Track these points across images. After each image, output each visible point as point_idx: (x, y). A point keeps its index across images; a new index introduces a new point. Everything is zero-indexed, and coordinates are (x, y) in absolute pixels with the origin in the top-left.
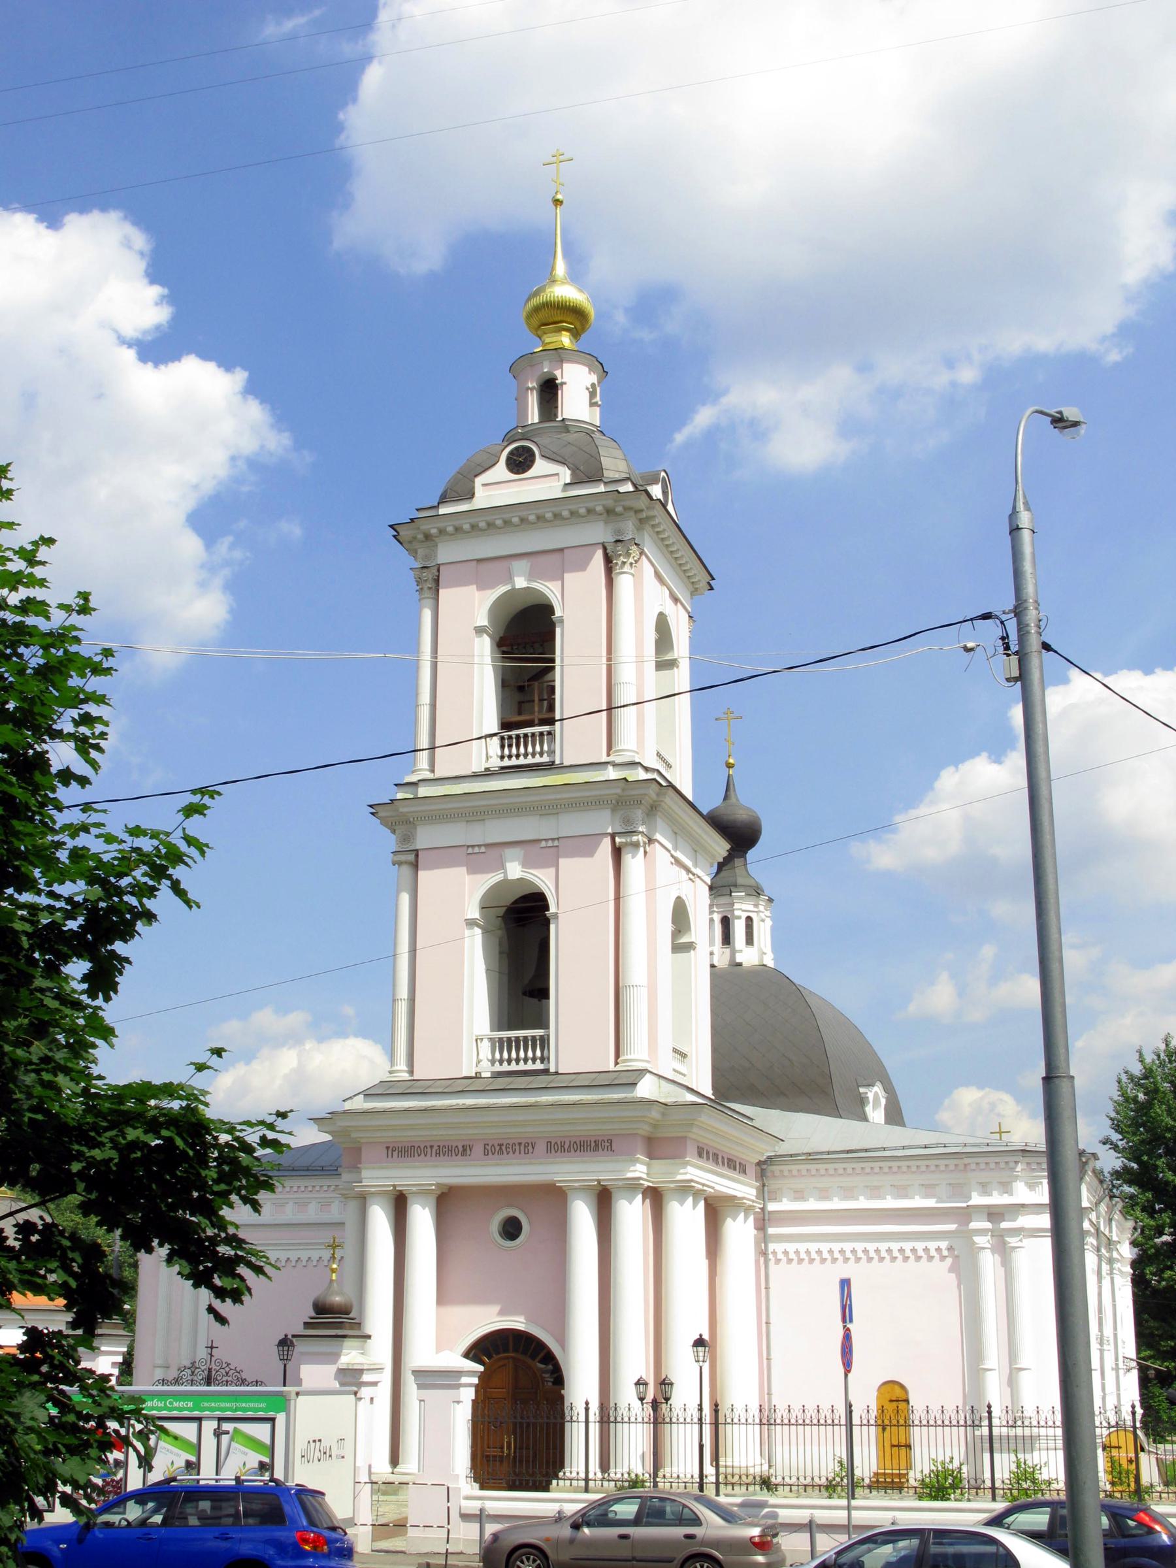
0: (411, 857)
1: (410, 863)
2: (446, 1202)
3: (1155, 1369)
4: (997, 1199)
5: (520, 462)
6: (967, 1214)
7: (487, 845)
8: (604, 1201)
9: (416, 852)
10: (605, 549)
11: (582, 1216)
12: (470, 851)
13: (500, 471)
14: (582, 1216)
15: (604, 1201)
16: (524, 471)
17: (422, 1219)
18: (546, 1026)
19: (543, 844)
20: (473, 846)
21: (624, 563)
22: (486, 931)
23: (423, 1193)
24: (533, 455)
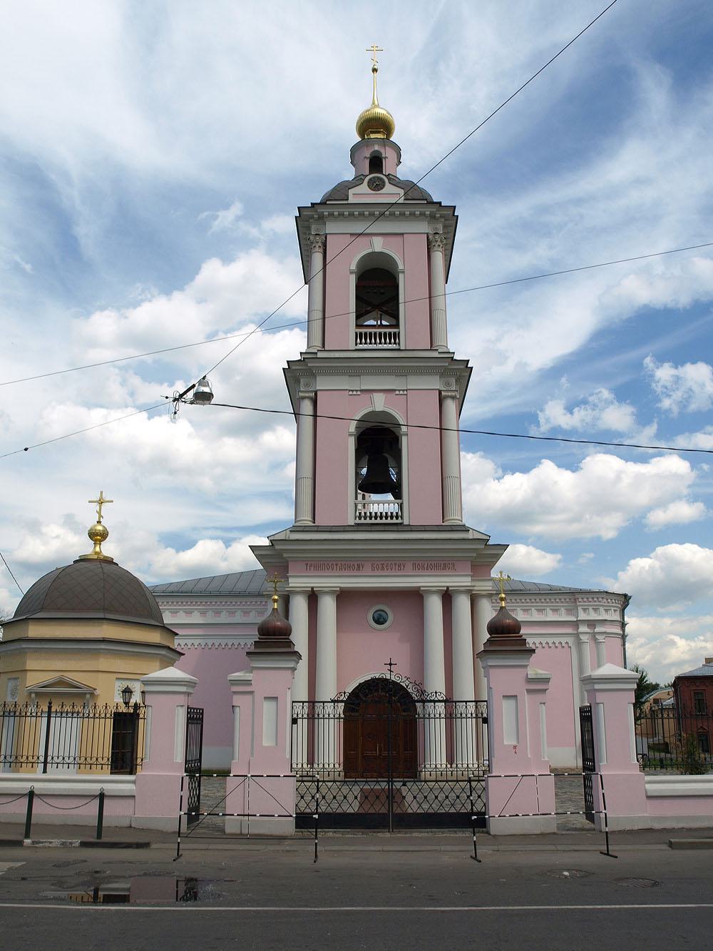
2: (344, 597)
4: (593, 616)
6: (576, 624)
7: (361, 391)
8: (447, 597)
11: (434, 606)
12: (351, 393)
14: (434, 606)
15: (447, 597)
17: (328, 606)
19: (397, 392)
20: (353, 391)
21: (439, 245)
23: (331, 592)
24: (384, 182)
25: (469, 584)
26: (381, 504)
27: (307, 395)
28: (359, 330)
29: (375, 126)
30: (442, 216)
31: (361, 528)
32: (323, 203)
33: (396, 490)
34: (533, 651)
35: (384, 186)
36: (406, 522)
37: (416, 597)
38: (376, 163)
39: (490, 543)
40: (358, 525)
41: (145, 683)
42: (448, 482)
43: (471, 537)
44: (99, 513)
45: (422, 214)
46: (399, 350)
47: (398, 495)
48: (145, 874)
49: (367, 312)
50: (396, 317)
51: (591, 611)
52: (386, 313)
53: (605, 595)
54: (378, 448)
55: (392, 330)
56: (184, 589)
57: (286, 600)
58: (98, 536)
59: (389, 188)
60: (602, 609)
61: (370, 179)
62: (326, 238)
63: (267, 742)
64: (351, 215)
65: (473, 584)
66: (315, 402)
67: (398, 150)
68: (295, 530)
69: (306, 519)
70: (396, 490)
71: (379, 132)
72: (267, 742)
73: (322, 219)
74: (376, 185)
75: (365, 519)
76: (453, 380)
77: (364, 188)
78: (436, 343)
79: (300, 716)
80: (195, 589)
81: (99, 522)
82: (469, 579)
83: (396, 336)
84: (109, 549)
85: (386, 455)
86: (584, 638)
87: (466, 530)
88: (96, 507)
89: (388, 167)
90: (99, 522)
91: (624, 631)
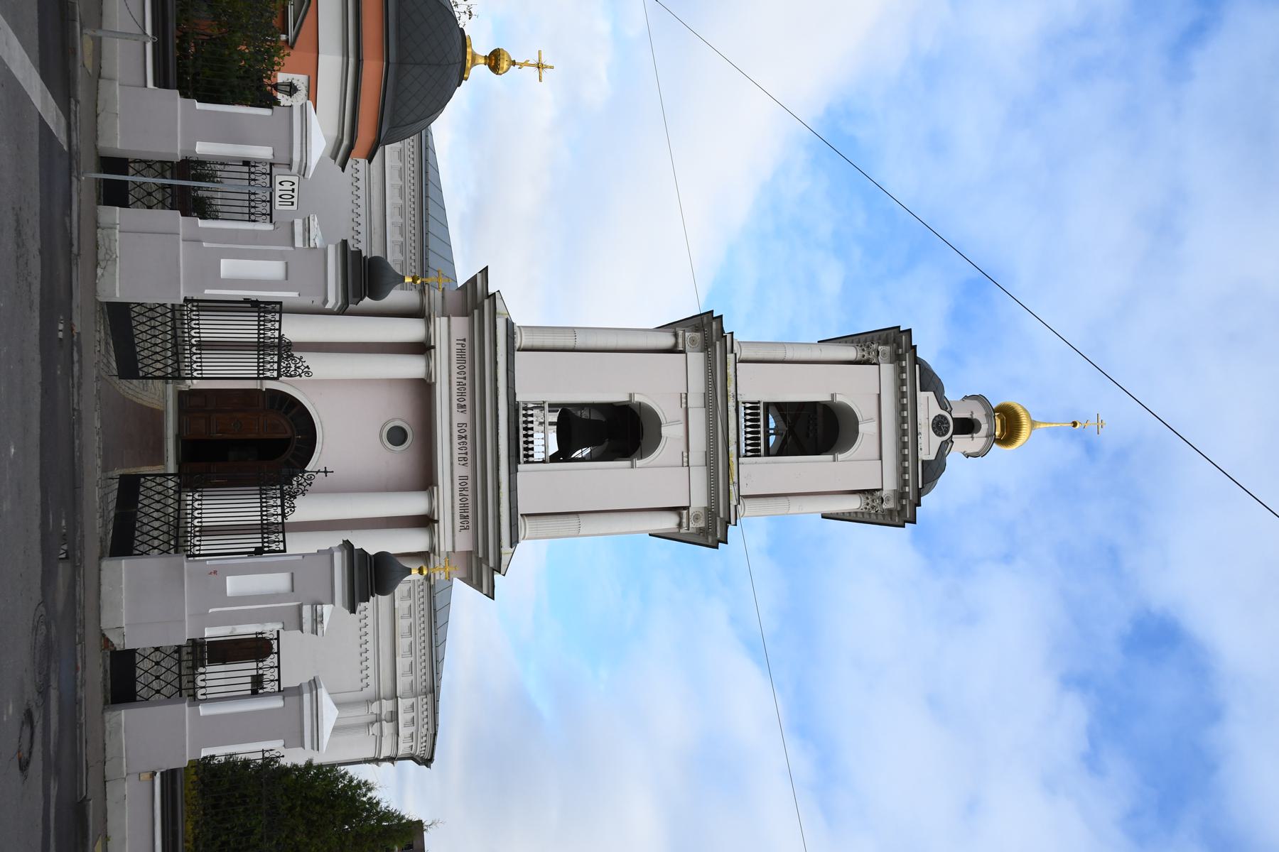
0: (681, 348)
1: (676, 344)
7: (687, 409)
8: (426, 522)
11: (415, 504)
14: (415, 504)
15: (426, 522)
17: (412, 367)
23: (429, 374)
25: (442, 549)
26: (545, 441)
27: (680, 340)
28: (762, 406)
29: (1009, 425)
30: (903, 507)
31: (513, 414)
32: (916, 360)
33: (563, 455)
34: (353, 611)
35: (939, 435)
36: (520, 467)
37: (426, 481)
38: (967, 426)
39: (497, 577)
40: (517, 411)
41: (303, 108)
42: (573, 521)
43: (503, 550)
44: (526, 64)
45: (905, 483)
46: (738, 456)
47: (554, 458)
49: (784, 417)
50: (782, 451)
51: (409, 716)
52: (784, 443)
53: (431, 732)
54: (613, 431)
55: (762, 447)
56: (430, 152)
57: (418, 313)
58: (495, 61)
59: (937, 441)
60: (413, 729)
61: (946, 418)
63: (228, 267)
64: (903, 395)
65: (443, 556)
66: (672, 350)
67: (982, 454)
68: (510, 325)
69: (522, 340)
70: (563, 455)
71: (1002, 430)
72: (228, 267)
73: (897, 358)
74: (939, 425)
75: (525, 415)
76: (701, 524)
77: (936, 410)
78: (747, 502)
79: (253, 170)
80: (430, 202)
81: (514, 63)
82: (449, 549)
83: (756, 453)
84: (479, 73)
85: (606, 444)
86: (375, 708)
87: (514, 542)
88: (534, 60)
89: (962, 443)
90: (514, 63)
91: (384, 760)
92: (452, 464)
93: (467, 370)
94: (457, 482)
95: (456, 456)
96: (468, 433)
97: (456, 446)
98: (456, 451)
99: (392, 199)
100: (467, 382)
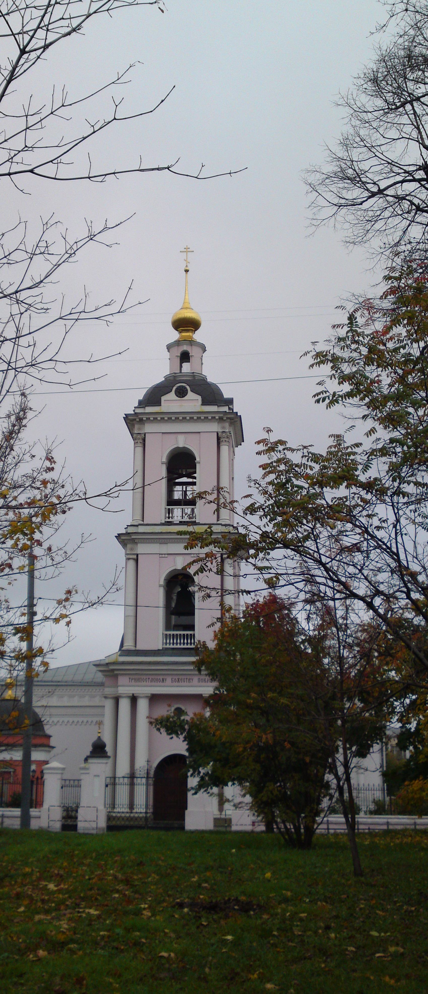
0: (135, 557)
1: (134, 559)
3: (81, 908)
5: (181, 393)
9: (137, 555)
10: (218, 434)
12: (161, 556)
13: (172, 395)
16: (183, 397)
17: (143, 705)
18: (194, 630)
22: (164, 589)
24: (187, 390)
35: (187, 393)
40: (167, 649)
48: (404, 232)
59: (191, 395)
62: (145, 435)
69: (129, 645)
92: (192, 686)
93: (145, 677)
94: (201, 684)
95: (188, 684)
96: (177, 678)
97: (183, 684)
98: (185, 684)
99: (75, 702)
100: (151, 677)
